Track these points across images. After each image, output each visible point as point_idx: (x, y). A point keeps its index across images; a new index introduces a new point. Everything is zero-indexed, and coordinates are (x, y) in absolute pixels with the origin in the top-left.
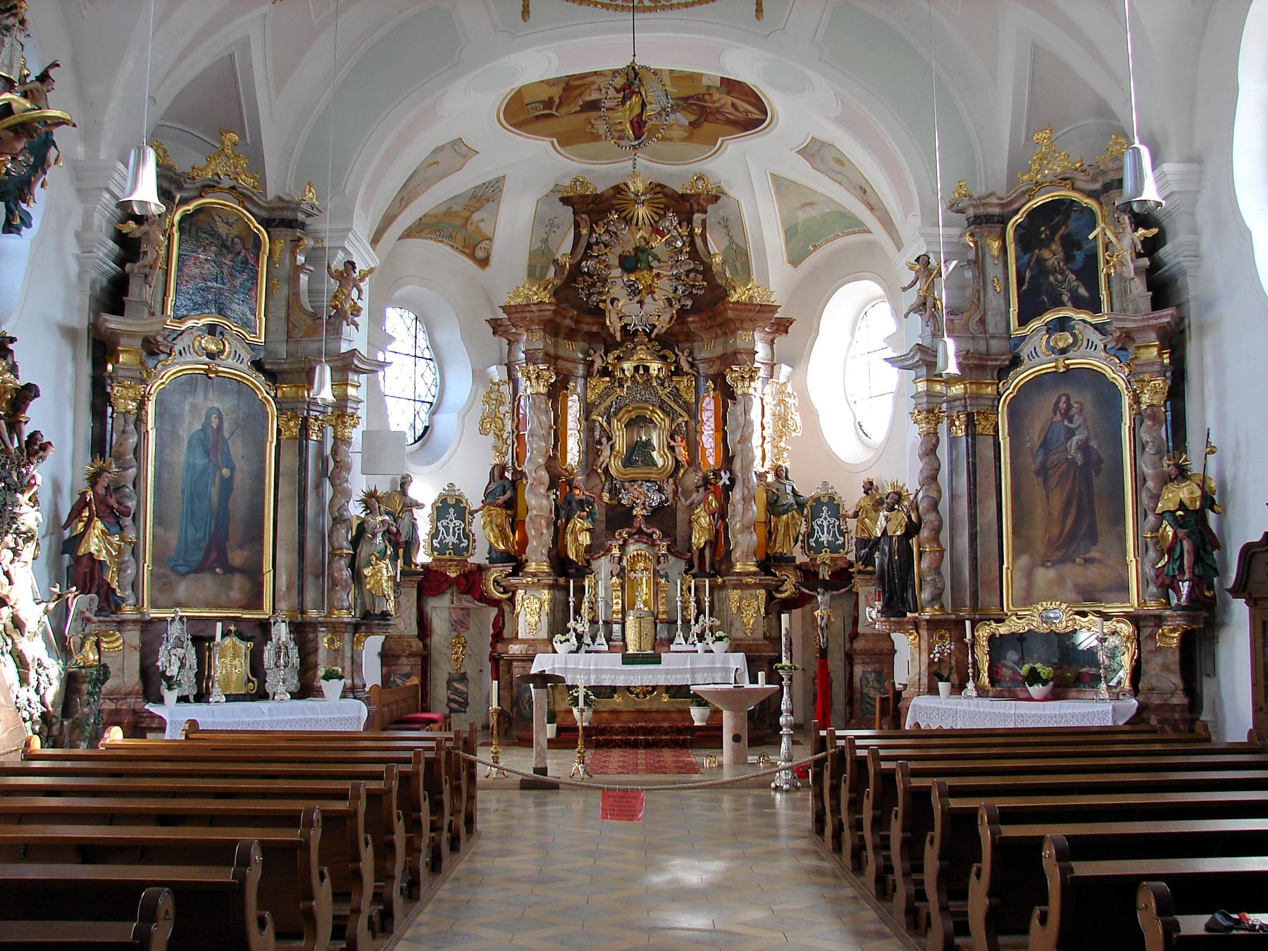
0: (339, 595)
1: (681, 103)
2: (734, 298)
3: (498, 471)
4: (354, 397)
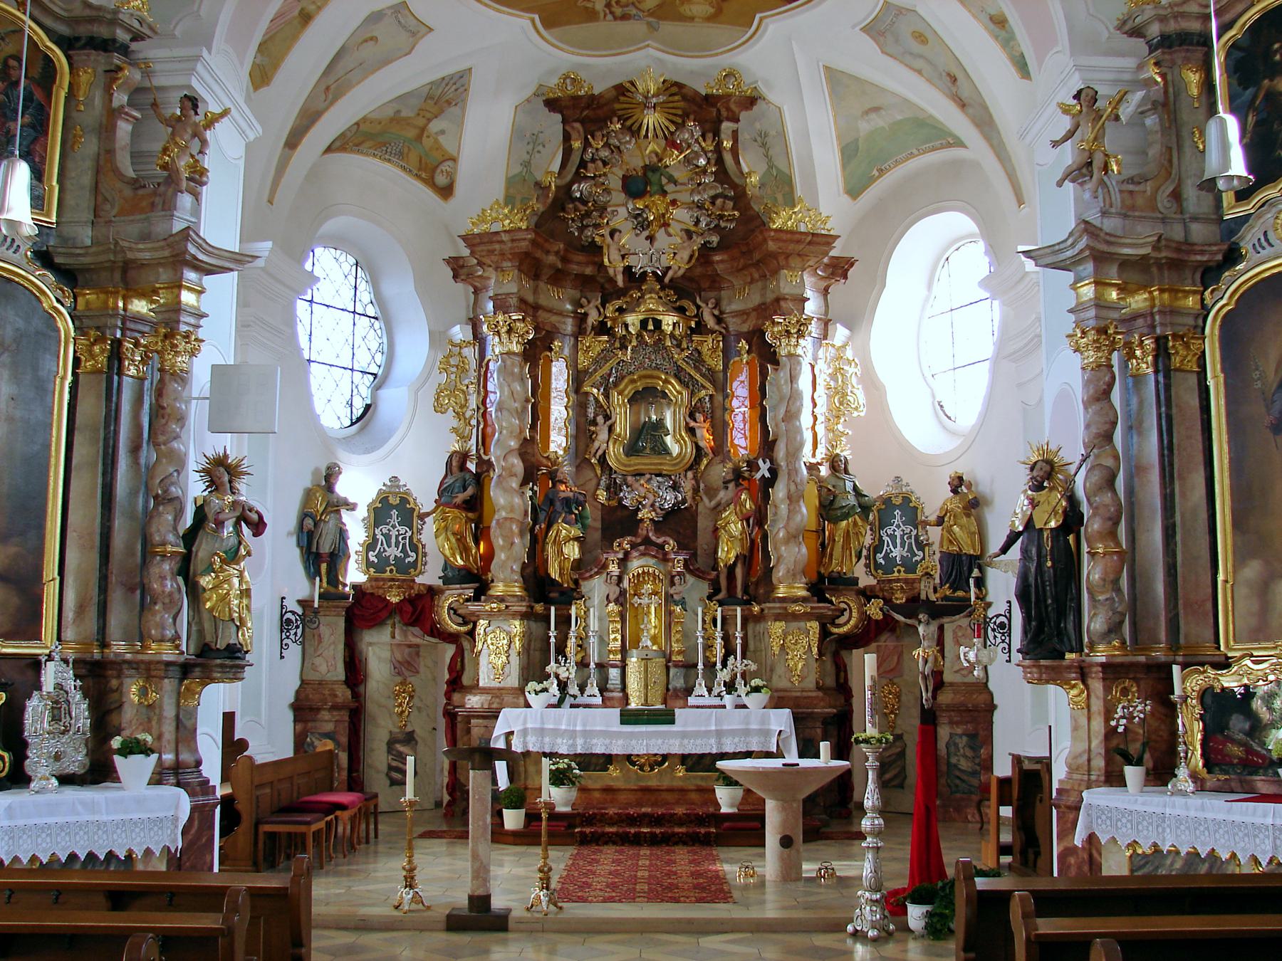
0: (158, 618)
3: (457, 462)
4: (193, 307)
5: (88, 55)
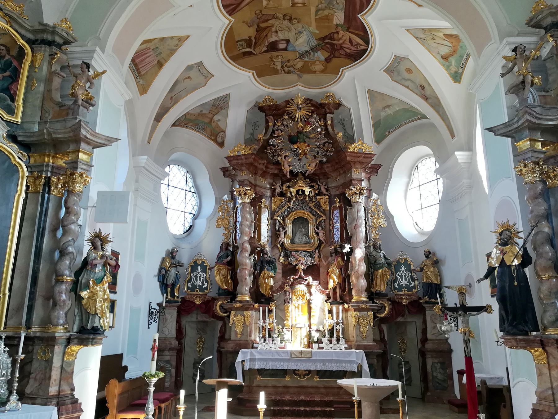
3: (225, 246)
5: (41, 47)
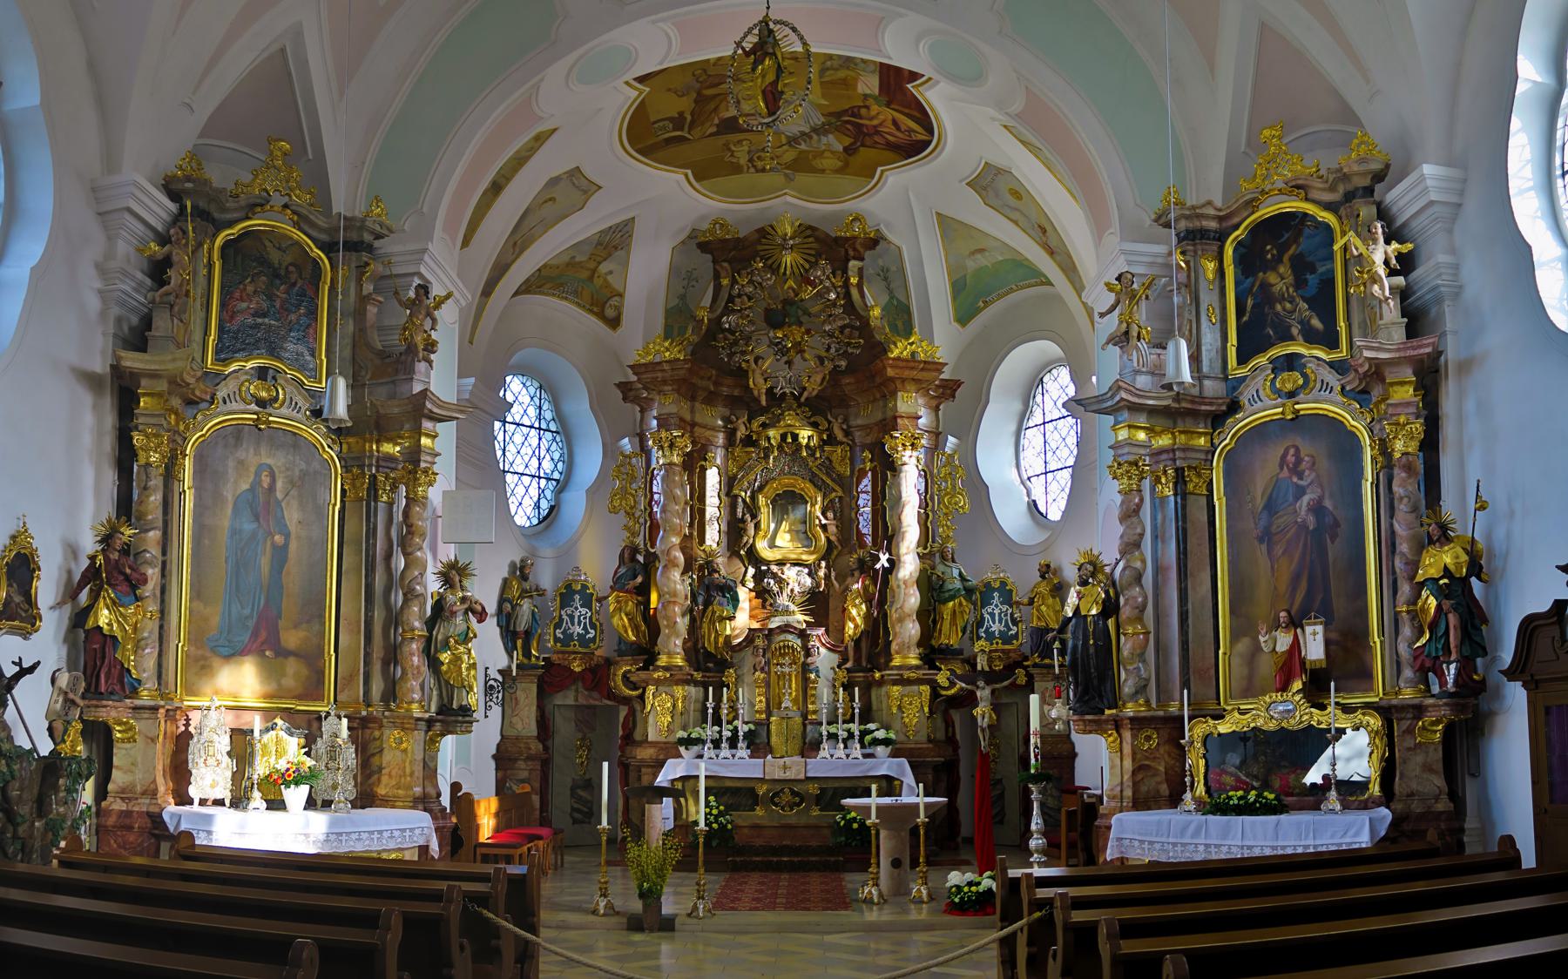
1: (833, 120)
2: (895, 353)
